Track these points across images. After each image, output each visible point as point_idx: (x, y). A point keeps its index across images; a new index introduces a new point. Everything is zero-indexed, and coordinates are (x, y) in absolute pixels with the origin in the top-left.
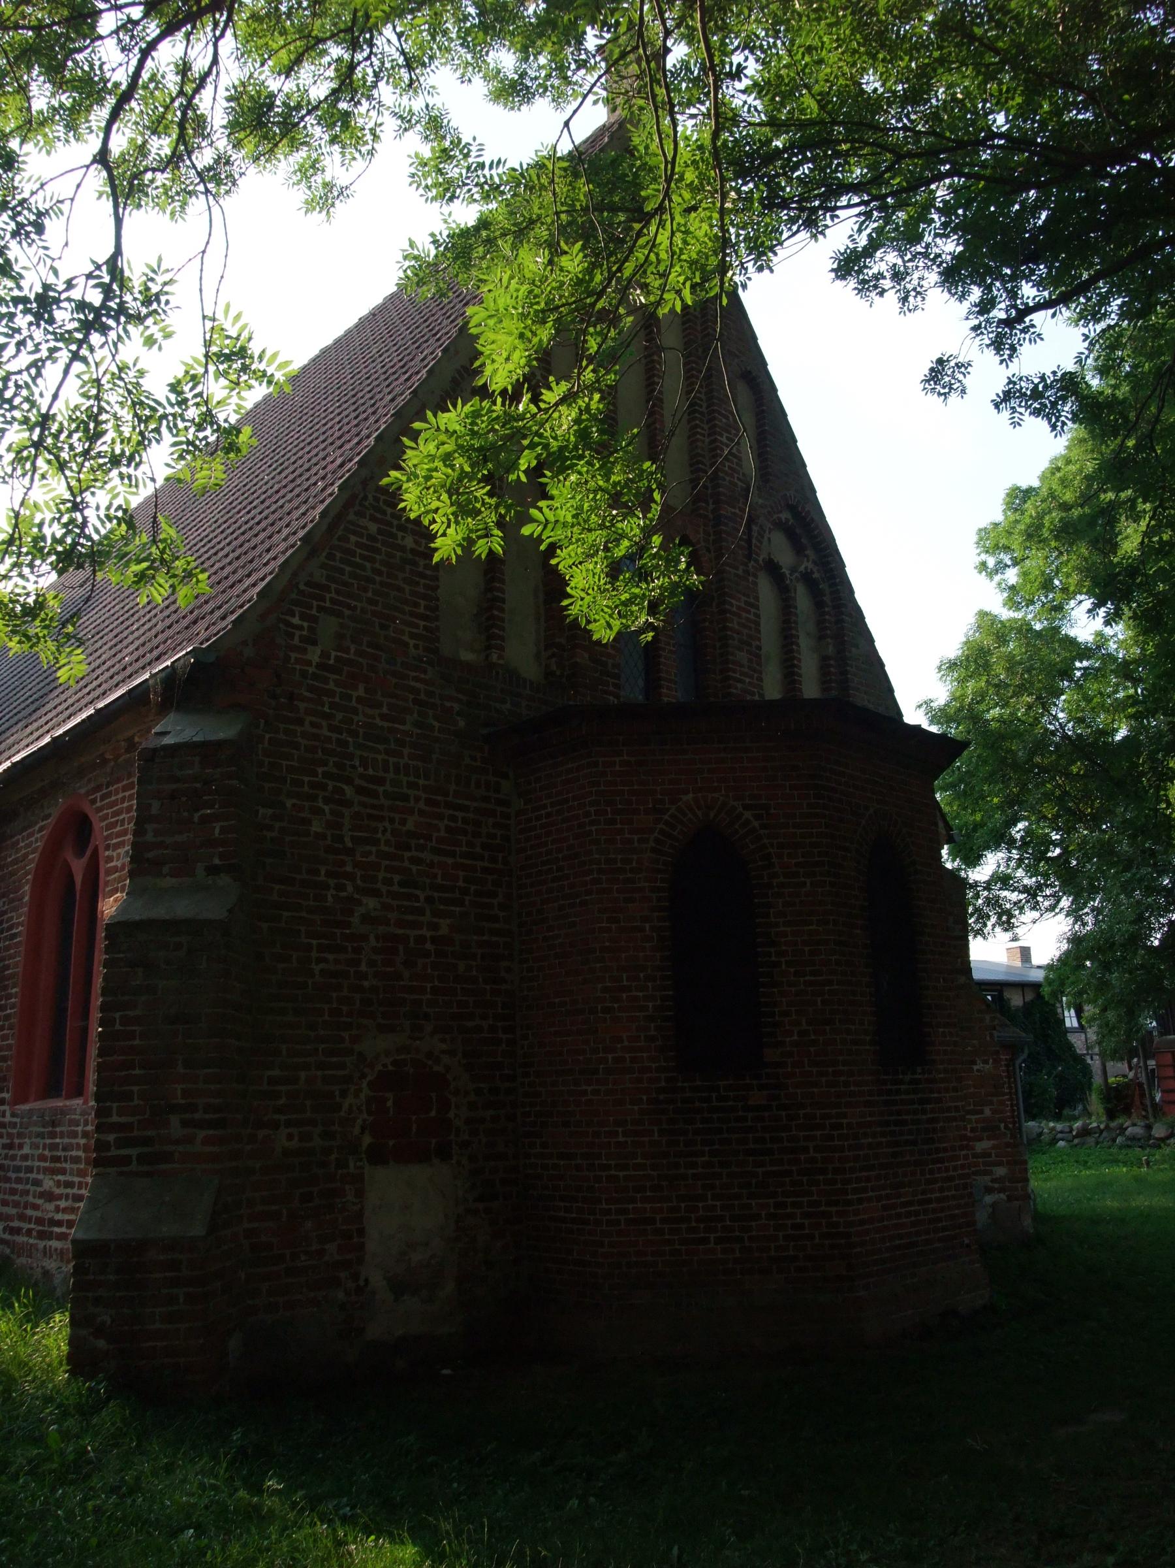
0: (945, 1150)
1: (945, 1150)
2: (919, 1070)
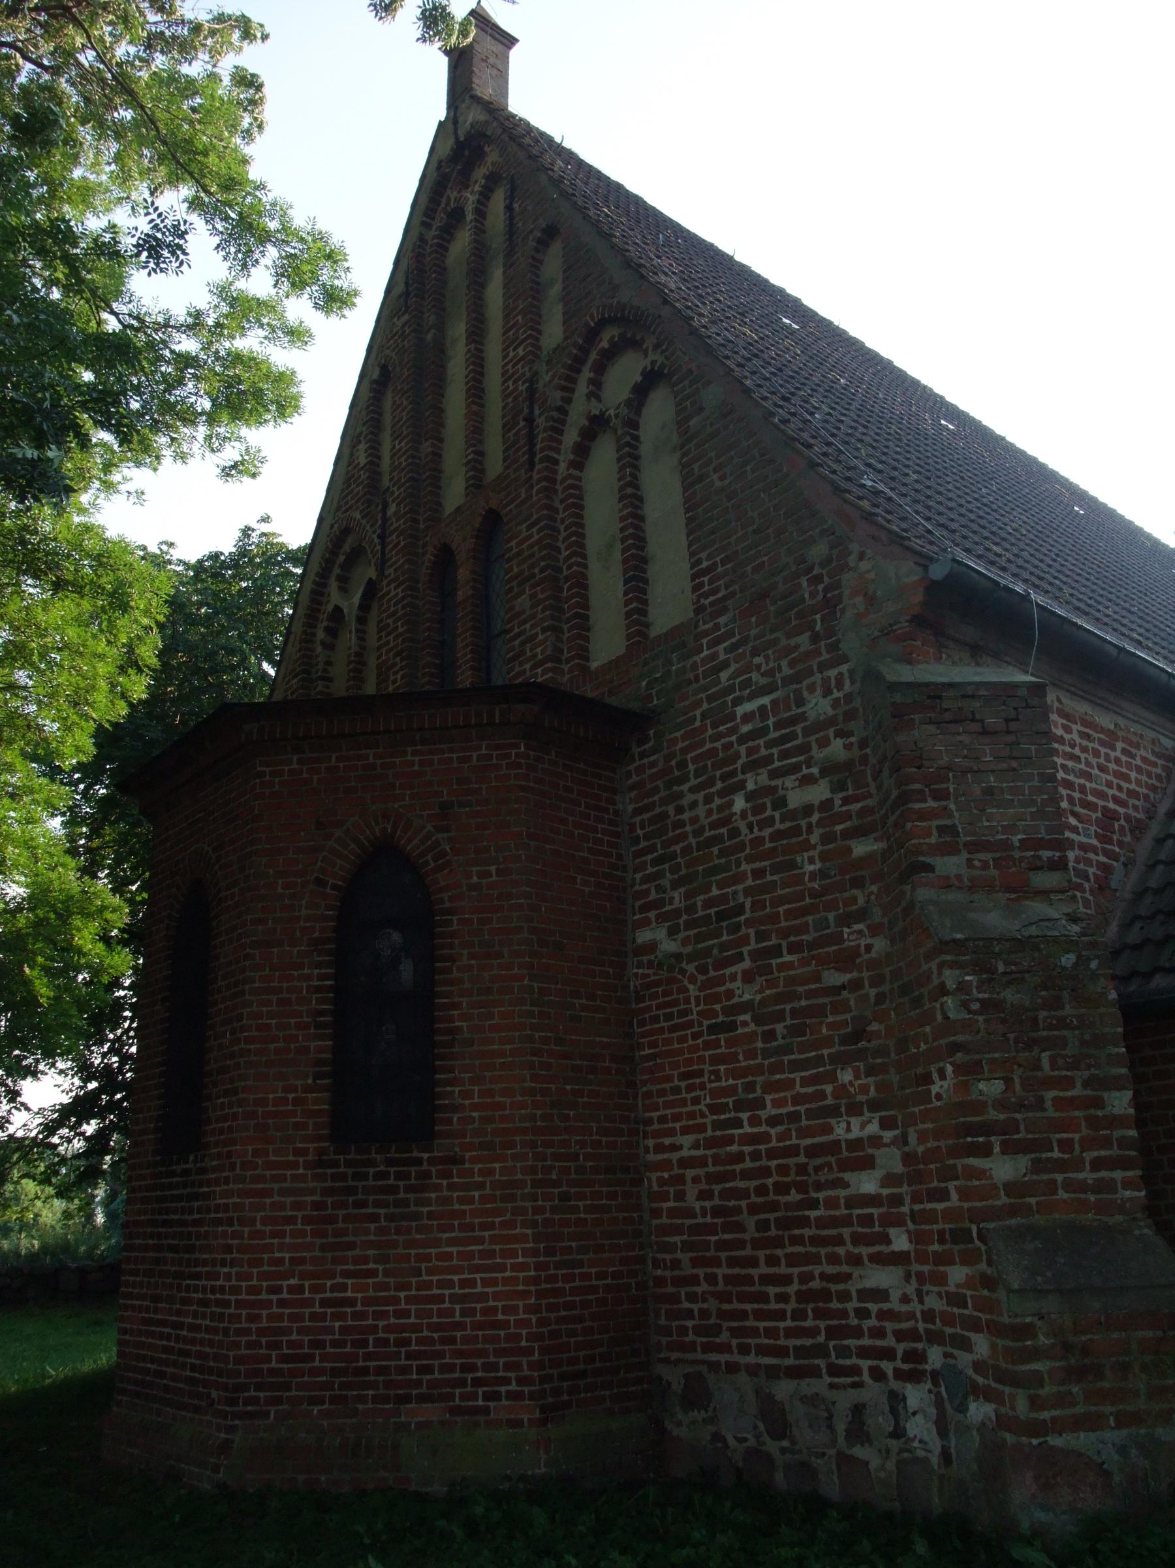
0: (205, 1263)
1: (205, 1263)
2: (191, 1158)
